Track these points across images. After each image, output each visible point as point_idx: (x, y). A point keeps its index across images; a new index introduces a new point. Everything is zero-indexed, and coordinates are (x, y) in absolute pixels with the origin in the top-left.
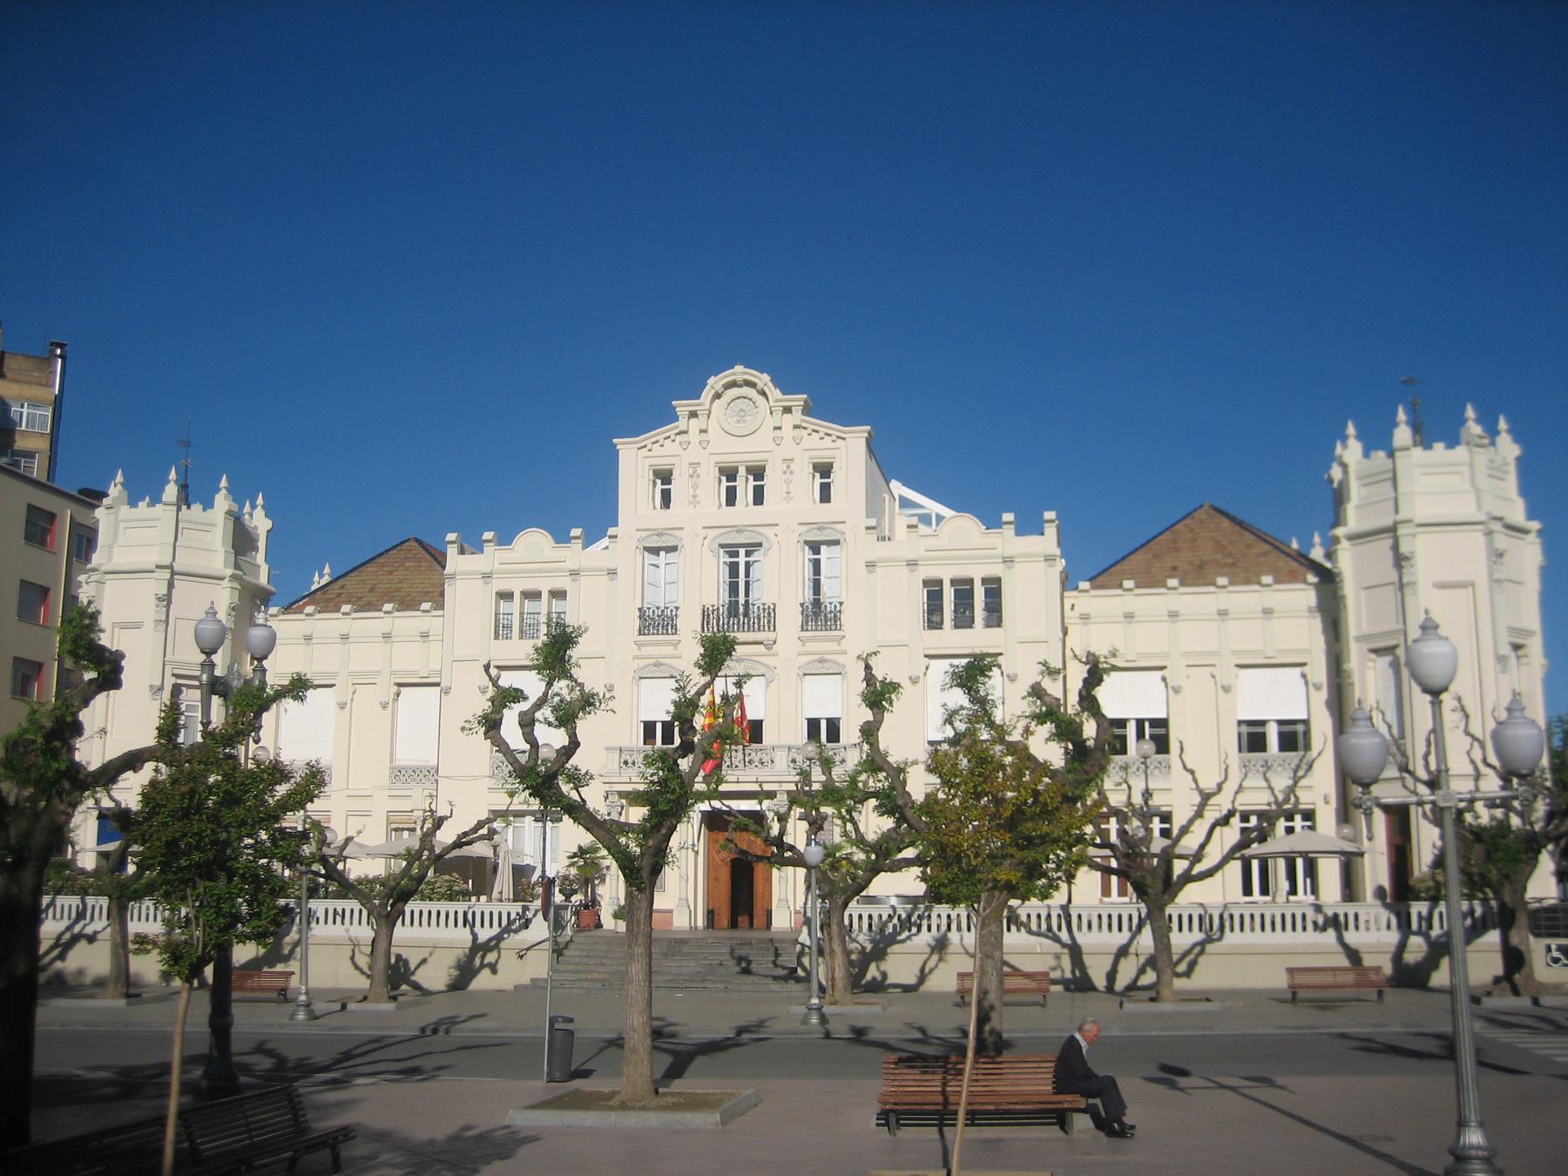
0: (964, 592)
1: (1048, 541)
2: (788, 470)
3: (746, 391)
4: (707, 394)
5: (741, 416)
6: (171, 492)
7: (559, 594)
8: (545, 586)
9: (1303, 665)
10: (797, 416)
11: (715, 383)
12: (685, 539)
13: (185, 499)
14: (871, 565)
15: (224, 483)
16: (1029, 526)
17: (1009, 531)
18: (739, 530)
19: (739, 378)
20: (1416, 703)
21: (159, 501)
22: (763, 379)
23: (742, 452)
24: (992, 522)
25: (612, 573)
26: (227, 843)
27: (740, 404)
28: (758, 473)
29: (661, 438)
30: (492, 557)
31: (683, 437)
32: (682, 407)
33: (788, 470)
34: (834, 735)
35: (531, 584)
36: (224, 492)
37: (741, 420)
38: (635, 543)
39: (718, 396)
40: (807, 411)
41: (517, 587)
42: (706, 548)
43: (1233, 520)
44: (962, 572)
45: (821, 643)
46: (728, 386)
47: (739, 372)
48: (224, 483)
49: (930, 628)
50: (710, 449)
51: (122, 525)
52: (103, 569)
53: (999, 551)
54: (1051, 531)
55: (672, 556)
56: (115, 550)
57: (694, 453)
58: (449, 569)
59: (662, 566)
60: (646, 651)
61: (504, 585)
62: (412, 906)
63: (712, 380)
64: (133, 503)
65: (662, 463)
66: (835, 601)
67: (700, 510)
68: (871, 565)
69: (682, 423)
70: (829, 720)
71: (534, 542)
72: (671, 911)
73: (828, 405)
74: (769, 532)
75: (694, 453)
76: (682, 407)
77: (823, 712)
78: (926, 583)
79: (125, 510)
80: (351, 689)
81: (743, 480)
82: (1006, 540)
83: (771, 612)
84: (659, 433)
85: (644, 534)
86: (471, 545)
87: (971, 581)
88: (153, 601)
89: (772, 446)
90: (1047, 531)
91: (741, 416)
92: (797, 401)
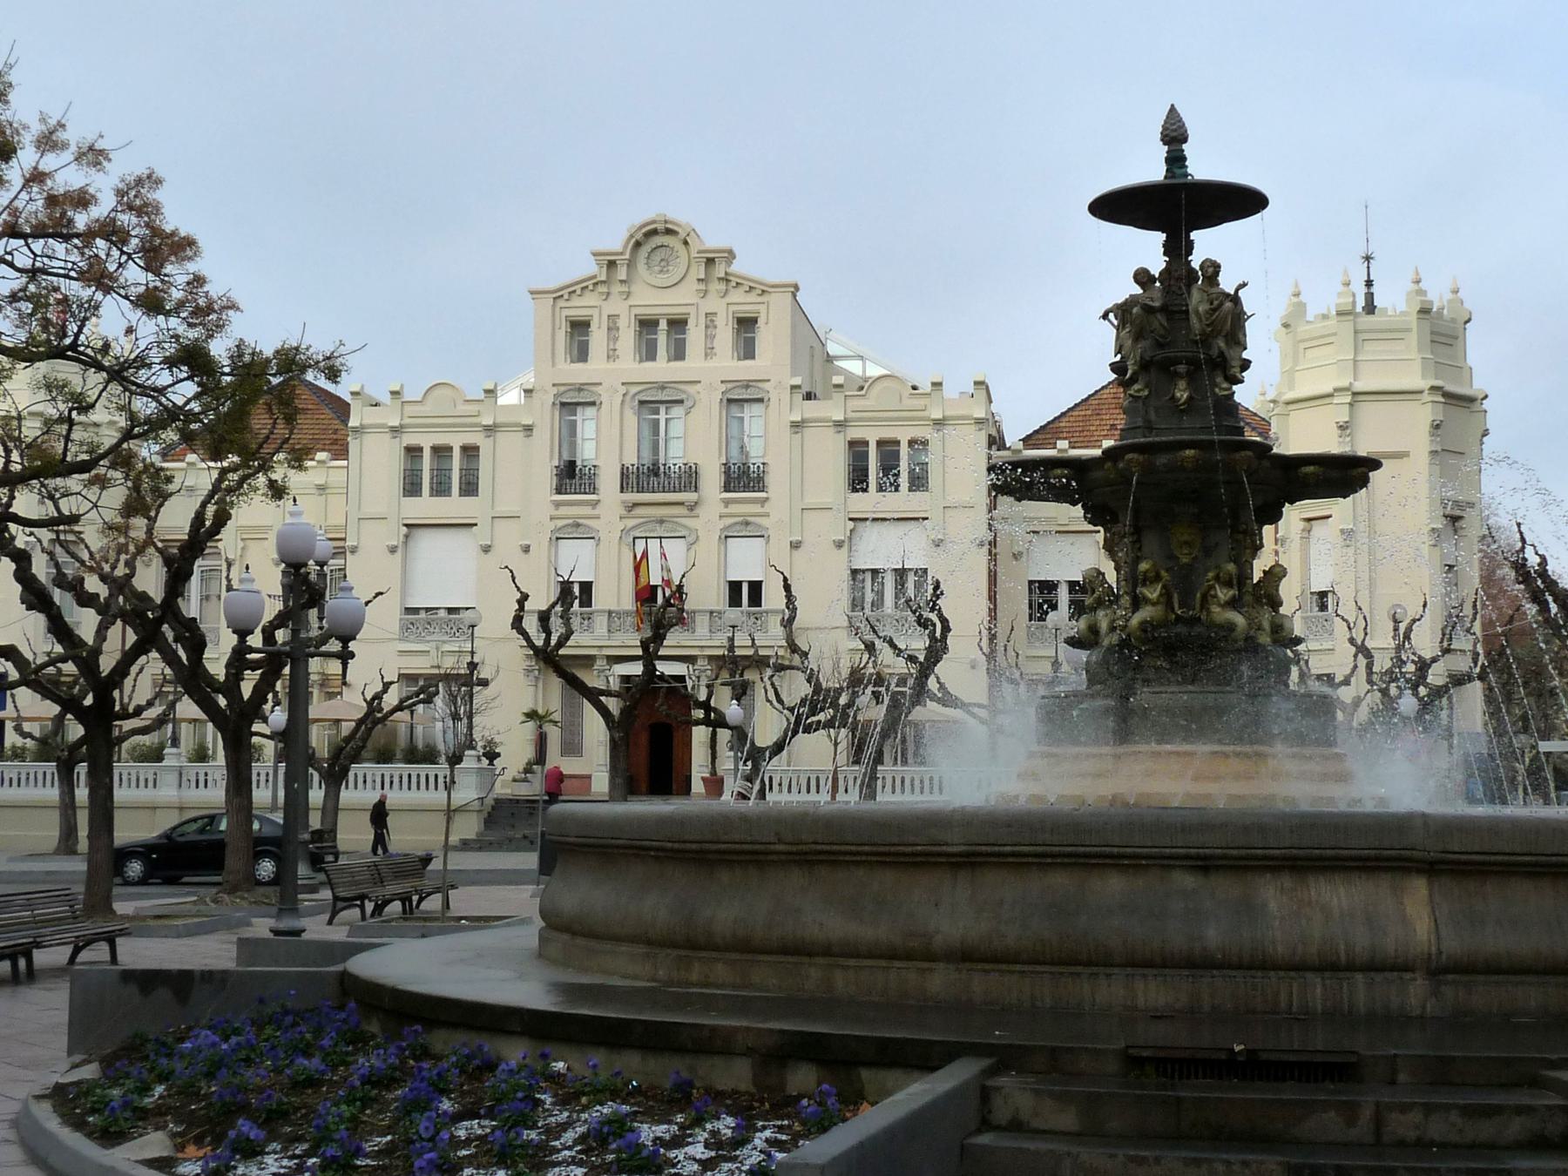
0: (889, 450)
2: (612, 329)
3: (658, 240)
12: (604, 394)
14: (797, 426)
25: (528, 429)
27: (657, 256)
33: (612, 329)
34: (756, 599)
42: (627, 406)
44: (441, 440)
45: (745, 504)
49: (855, 490)
50: (631, 302)
57: (612, 307)
60: (733, 509)
61: (410, 439)
62: (356, 769)
66: (589, 464)
70: (751, 583)
72: (589, 777)
74: (691, 389)
77: (745, 574)
78: (852, 444)
80: (241, 544)
83: (592, 477)
85: (730, 386)
87: (420, 449)
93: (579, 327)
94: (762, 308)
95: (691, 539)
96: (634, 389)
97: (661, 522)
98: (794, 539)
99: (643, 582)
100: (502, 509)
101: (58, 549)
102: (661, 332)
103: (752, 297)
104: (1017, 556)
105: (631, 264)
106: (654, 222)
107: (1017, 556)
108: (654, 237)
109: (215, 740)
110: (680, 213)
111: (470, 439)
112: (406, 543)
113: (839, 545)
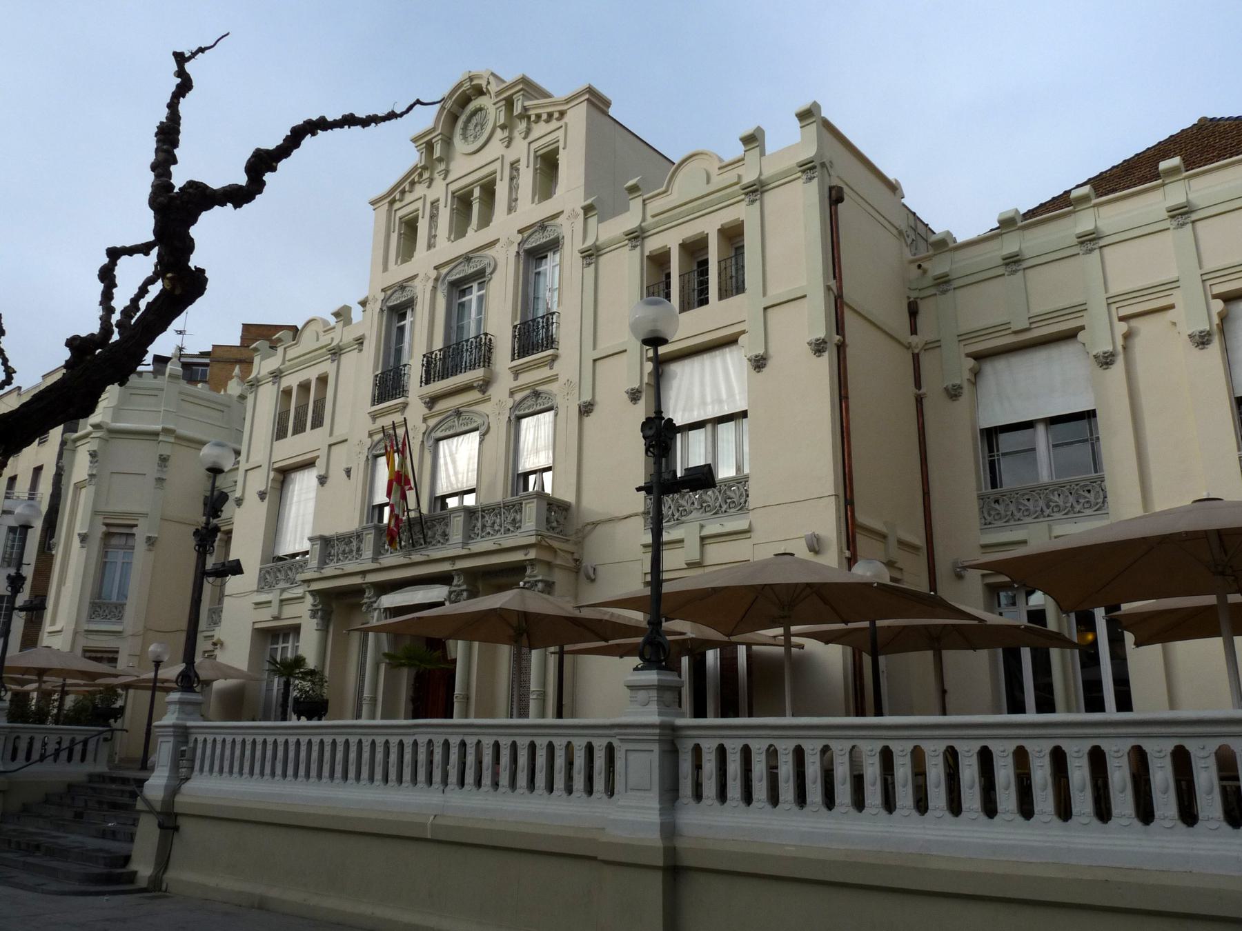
74: (490, 252)
93: (410, 226)
94: (560, 133)
95: (483, 429)
96: (444, 271)
97: (458, 413)
98: (949, 383)
99: (1001, 271)
100: (777, 292)
101: (724, 396)
102: (473, 203)
103: (554, 124)
104: (954, 393)
105: (448, 142)
106: (460, 85)
107: (954, 393)
108: (462, 104)
109: (99, 685)
110: (480, 66)
111: (726, 217)
112: (1222, 330)
113: (1202, 340)
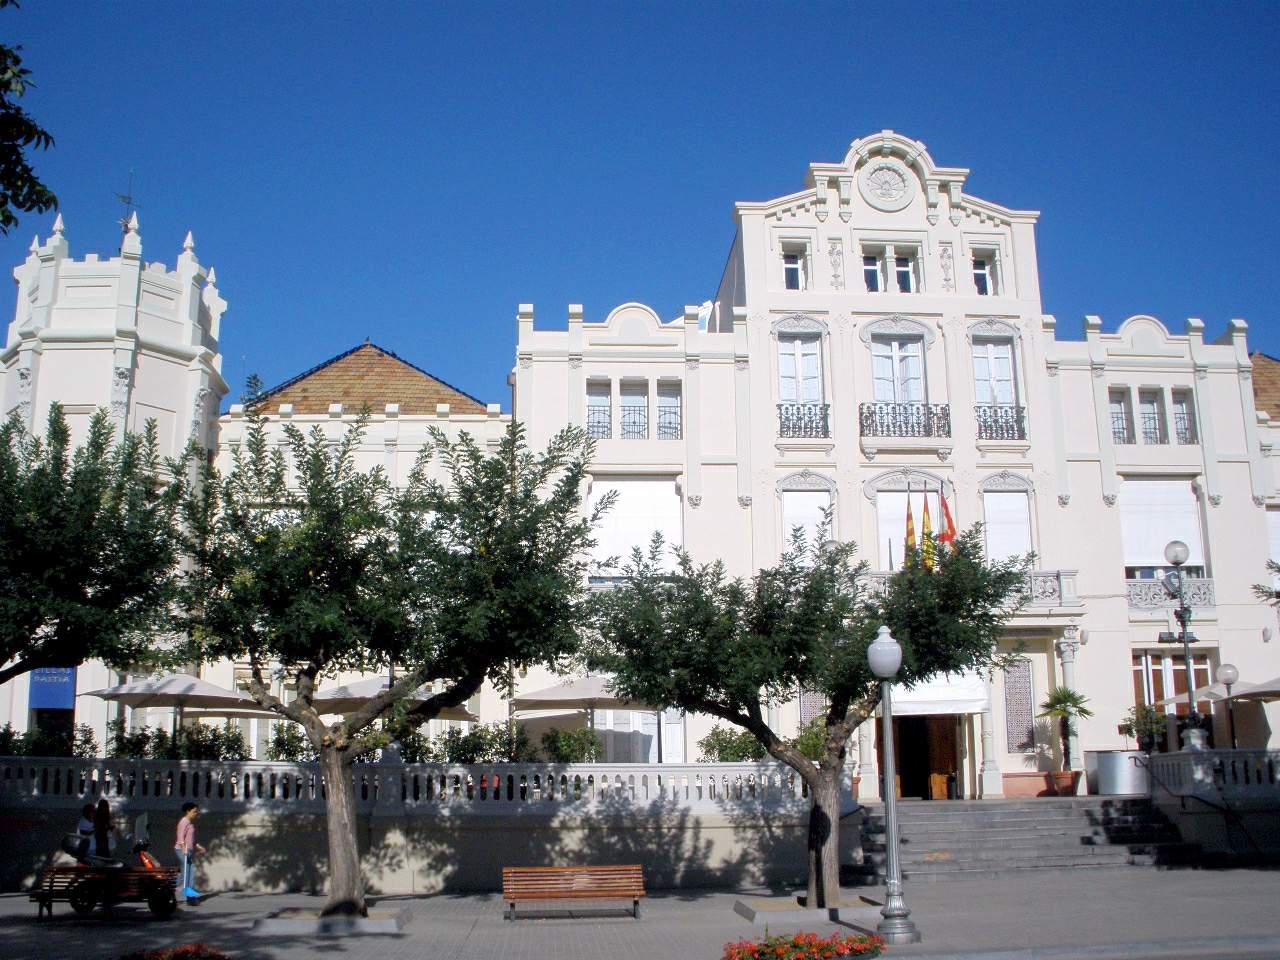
1: (1237, 351)
3: (892, 161)
4: (851, 159)
5: (885, 189)
6: (132, 243)
7: (671, 388)
8: (653, 374)
9: (1193, 476)
10: (957, 194)
11: (860, 146)
13: (145, 259)
14: (1052, 367)
15: (189, 241)
16: (1219, 335)
17: (1196, 339)
18: (896, 318)
19: (888, 144)
20: (878, 461)
21: (118, 252)
22: (917, 149)
23: (891, 230)
24: (1178, 327)
25: (742, 360)
26: (95, 491)
27: (887, 176)
28: (906, 256)
29: (806, 201)
30: (579, 335)
31: (820, 207)
32: (821, 171)
35: (634, 371)
36: (189, 254)
37: (881, 192)
38: (770, 327)
39: (860, 164)
40: (967, 188)
41: (615, 374)
43: (352, 352)
46: (895, 153)
47: (888, 137)
48: (189, 241)
51: (63, 283)
52: (43, 333)
53: (1187, 359)
54: (1240, 340)
55: (814, 347)
56: (54, 312)
58: (521, 348)
59: (896, 360)
63: (856, 144)
64: (78, 255)
65: (795, 235)
67: (835, 288)
68: (1052, 367)
69: (821, 189)
71: (633, 320)
73: (994, 184)
74: (931, 322)
75: (833, 226)
76: (821, 171)
79: (68, 264)
81: (891, 262)
82: (1195, 347)
84: (791, 200)
86: (552, 319)
88: (112, 376)
89: (926, 225)
90: (1235, 339)
91: (885, 189)
92: (958, 175)
